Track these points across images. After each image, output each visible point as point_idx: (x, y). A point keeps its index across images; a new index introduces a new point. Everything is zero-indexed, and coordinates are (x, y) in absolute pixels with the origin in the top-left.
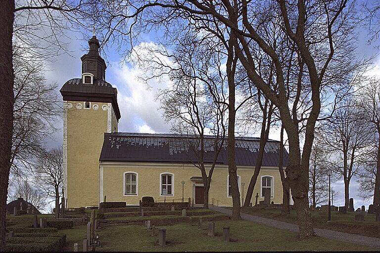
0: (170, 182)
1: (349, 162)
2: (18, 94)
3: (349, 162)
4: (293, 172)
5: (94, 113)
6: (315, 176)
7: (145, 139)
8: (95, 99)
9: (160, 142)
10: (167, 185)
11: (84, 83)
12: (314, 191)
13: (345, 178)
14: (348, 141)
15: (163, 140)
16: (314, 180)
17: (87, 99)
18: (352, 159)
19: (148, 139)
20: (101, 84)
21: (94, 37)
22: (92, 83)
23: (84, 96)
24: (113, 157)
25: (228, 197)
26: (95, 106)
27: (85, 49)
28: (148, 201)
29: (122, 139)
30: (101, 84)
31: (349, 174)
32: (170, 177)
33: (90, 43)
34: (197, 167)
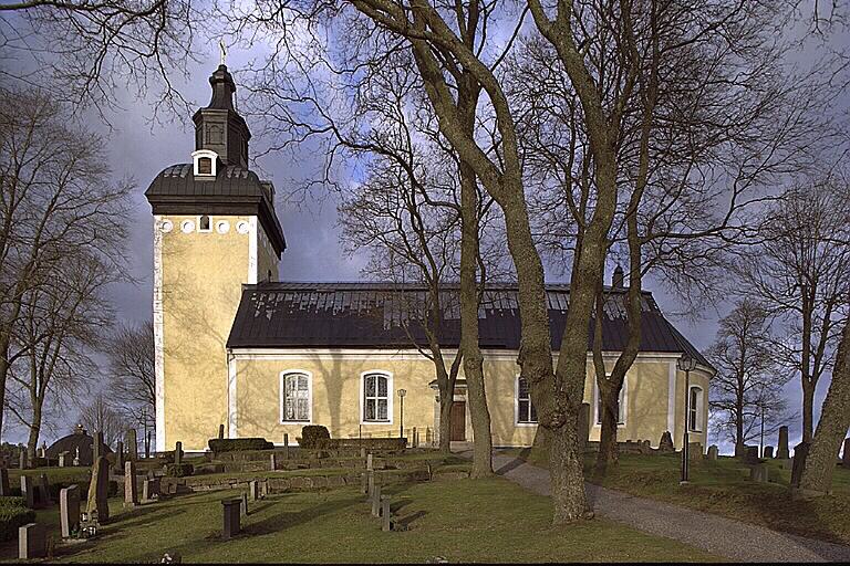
0: (384, 392)
1: (815, 339)
2: (53, 204)
3: (815, 339)
4: (531, 365)
5: (220, 241)
6: (743, 372)
7: (330, 297)
8: (220, 210)
9: (363, 302)
10: (377, 398)
11: (196, 172)
12: (740, 411)
13: (805, 376)
14: (814, 286)
15: (372, 296)
16: (740, 382)
17: (205, 210)
18: (826, 329)
19: (339, 296)
20: (233, 175)
21: (223, 68)
22: (214, 173)
23: (231, 204)
24: (355, 339)
25: (282, 423)
26: (223, 224)
27: (204, 96)
28: (314, 435)
29: (280, 297)
30: (233, 175)
31: (816, 368)
32: (383, 381)
33: (213, 82)
34: (426, 355)
